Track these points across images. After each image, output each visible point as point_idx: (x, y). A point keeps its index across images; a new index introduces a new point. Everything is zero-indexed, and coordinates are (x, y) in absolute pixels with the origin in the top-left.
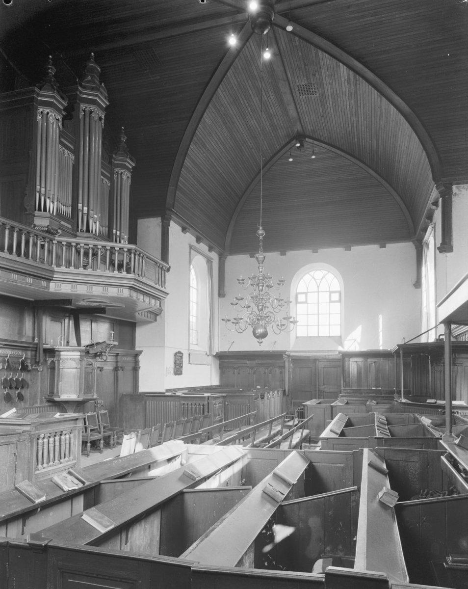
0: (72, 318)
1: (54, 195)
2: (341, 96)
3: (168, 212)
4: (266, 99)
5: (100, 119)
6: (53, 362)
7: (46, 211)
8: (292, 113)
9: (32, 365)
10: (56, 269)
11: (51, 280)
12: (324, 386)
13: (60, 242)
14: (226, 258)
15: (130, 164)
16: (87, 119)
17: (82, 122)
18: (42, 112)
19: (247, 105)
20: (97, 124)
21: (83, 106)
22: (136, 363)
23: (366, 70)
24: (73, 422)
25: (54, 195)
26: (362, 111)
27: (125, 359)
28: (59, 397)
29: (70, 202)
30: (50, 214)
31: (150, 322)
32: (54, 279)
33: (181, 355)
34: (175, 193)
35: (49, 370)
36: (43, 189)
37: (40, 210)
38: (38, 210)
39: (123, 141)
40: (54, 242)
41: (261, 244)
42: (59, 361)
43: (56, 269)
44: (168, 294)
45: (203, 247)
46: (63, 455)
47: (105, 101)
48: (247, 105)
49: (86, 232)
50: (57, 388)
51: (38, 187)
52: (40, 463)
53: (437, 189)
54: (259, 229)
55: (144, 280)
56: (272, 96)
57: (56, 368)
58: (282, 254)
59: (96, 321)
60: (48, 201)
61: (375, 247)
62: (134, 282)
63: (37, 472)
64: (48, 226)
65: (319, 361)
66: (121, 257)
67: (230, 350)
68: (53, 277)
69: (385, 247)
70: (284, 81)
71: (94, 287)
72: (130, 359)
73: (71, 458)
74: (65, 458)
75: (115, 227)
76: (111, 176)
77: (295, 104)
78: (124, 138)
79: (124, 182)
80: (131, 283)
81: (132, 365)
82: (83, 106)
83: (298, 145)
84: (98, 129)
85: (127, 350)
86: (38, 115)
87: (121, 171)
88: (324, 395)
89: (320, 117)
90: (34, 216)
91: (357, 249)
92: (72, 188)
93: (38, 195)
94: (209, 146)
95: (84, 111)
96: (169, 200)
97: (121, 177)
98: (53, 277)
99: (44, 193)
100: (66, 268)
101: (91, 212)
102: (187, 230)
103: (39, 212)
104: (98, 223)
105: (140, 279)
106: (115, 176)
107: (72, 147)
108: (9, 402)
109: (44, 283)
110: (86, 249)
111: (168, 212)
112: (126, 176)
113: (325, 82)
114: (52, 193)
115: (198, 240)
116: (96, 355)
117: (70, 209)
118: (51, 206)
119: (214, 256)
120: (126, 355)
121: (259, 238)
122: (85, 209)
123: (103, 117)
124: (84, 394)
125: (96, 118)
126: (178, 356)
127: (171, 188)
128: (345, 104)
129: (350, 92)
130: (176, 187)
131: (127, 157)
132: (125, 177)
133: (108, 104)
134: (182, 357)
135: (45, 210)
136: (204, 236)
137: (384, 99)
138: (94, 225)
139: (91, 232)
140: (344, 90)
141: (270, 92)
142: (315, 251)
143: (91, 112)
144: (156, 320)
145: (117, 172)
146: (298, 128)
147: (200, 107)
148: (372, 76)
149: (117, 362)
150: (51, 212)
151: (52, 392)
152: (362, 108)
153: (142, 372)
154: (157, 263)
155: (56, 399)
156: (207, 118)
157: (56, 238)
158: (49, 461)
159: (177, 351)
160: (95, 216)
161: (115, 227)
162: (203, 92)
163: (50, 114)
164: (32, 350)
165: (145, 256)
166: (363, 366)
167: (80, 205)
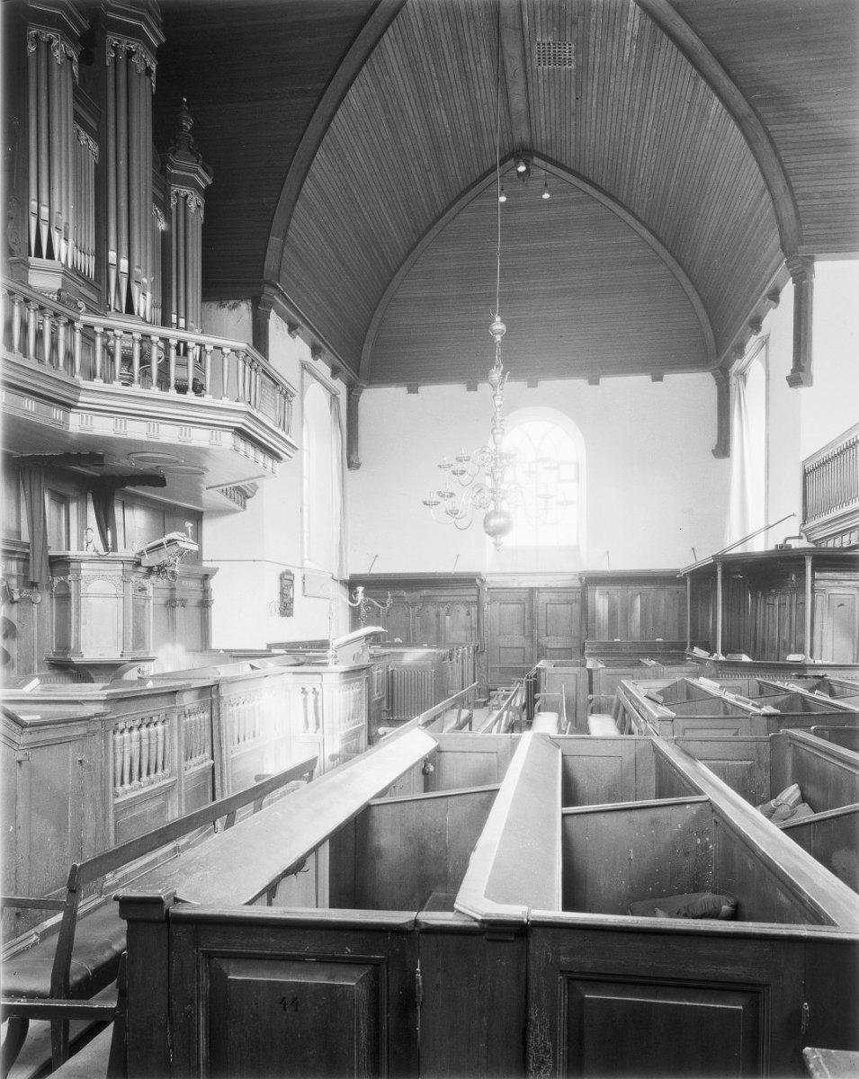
0: (90, 496)
1: (67, 224)
2: (619, 72)
3: (268, 290)
4: (473, 67)
5: (148, 71)
6: (65, 585)
7: (41, 257)
8: (518, 102)
9: (20, 592)
10: (84, 384)
11: (71, 406)
12: (547, 639)
13: (89, 327)
14: (360, 393)
15: (204, 179)
16: (122, 68)
17: (111, 71)
18: (37, 37)
19: (434, 75)
20: (142, 80)
21: (113, 39)
22: (206, 591)
23: (679, 20)
24: (166, 698)
25: (67, 224)
26: (653, 107)
27: (186, 583)
28: (82, 656)
29: (92, 247)
30: (63, 266)
31: (233, 511)
32: (79, 404)
33: (291, 578)
34: (282, 250)
35: (54, 600)
36: (45, 210)
37: (39, 254)
38: (47, 258)
39: (186, 127)
40: (76, 324)
41: (498, 351)
42: (78, 581)
43: (84, 384)
44: (297, 449)
45: (322, 367)
46: (152, 767)
47: (157, 31)
48: (434, 75)
49: (126, 313)
50: (78, 639)
51: (34, 204)
52: (118, 783)
53: (788, 267)
54: (493, 321)
55: (259, 416)
56: (485, 61)
57: (73, 596)
58: (469, 389)
59: (132, 506)
60: (56, 235)
61: (644, 380)
62: (246, 418)
63: (118, 800)
64: (59, 290)
65: (539, 592)
66: (182, 374)
67: (372, 572)
68: (78, 401)
69: (661, 380)
70: (515, 29)
71: (162, 426)
72: (195, 584)
73: (167, 771)
74: (156, 771)
75: (174, 310)
76: (165, 198)
77: (527, 83)
78: (188, 120)
79: (190, 216)
80: (238, 420)
81: (198, 596)
82: (113, 39)
83: (522, 169)
84: (144, 93)
85: (189, 567)
86: (30, 43)
87: (185, 191)
88: (548, 654)
89: (568, 114)
90: (28, 266)
91: (608, 382)
92: (96, 220)
93: (33, 221)
94: (351, 160)
95: (115, 49)
96: (271, 263)
97: (185, 204)
98: (78, 401)
99: (47, 219)
100: (105, 382)
101: (136, 269)
102: (298, 330)
103: (49, 261)
104: (149, 294)
105: (254, 412)
106: (173, 203)
107: (94, 125)
108: (174, 640)
109: (57, 413)
110: (127, 348)
111: (268, 290)
112: (195, 202)
113: (592, 40)
114: (64, 221)
115: (316, 351)
116: (150, 570)
117: (92, 261)
118: (63, 248)
119: (340, 386)
120: (189, 577)
121: (495, 339)
122: (124, 263)
123: (154, 68)
124: (134, 649)
125: (141, 69)
126: (286, 580)
127: (275, 241)
128: (622, 91)
129: (637, 65)
130: (284, 238)
131: (197, 163)
132: (192, 205)
133: (163, 40)
134: (292, 581)
135: (50, 255)
136: (326, 345)
137: (703, 83)
138: (142, 299)
139: (136, 312)
140: (626, 59)
141: (482, 50)
142: (533, 384)
143: (130, 54)
144: (244, 507)
145: (177, 194)
146: (522, 135)
147: (345, 70)
148: (688, 34)
149: (173, 589)
150: (63, 261)
151: (64, 646)
152: (654, 101)
153: (216, 612)
154: (277, 384)
155: (76, 660)
156: (353, 98)
157: (82, 318)
158: (131, 780)
159: (284, 569)
160: (145, 280)
161: (174, 310)
162: (355, 37)
163: (55, 42)
164: (18, 559)
165: (260, 368)
166: (619, 602)
167: (112, 255)
